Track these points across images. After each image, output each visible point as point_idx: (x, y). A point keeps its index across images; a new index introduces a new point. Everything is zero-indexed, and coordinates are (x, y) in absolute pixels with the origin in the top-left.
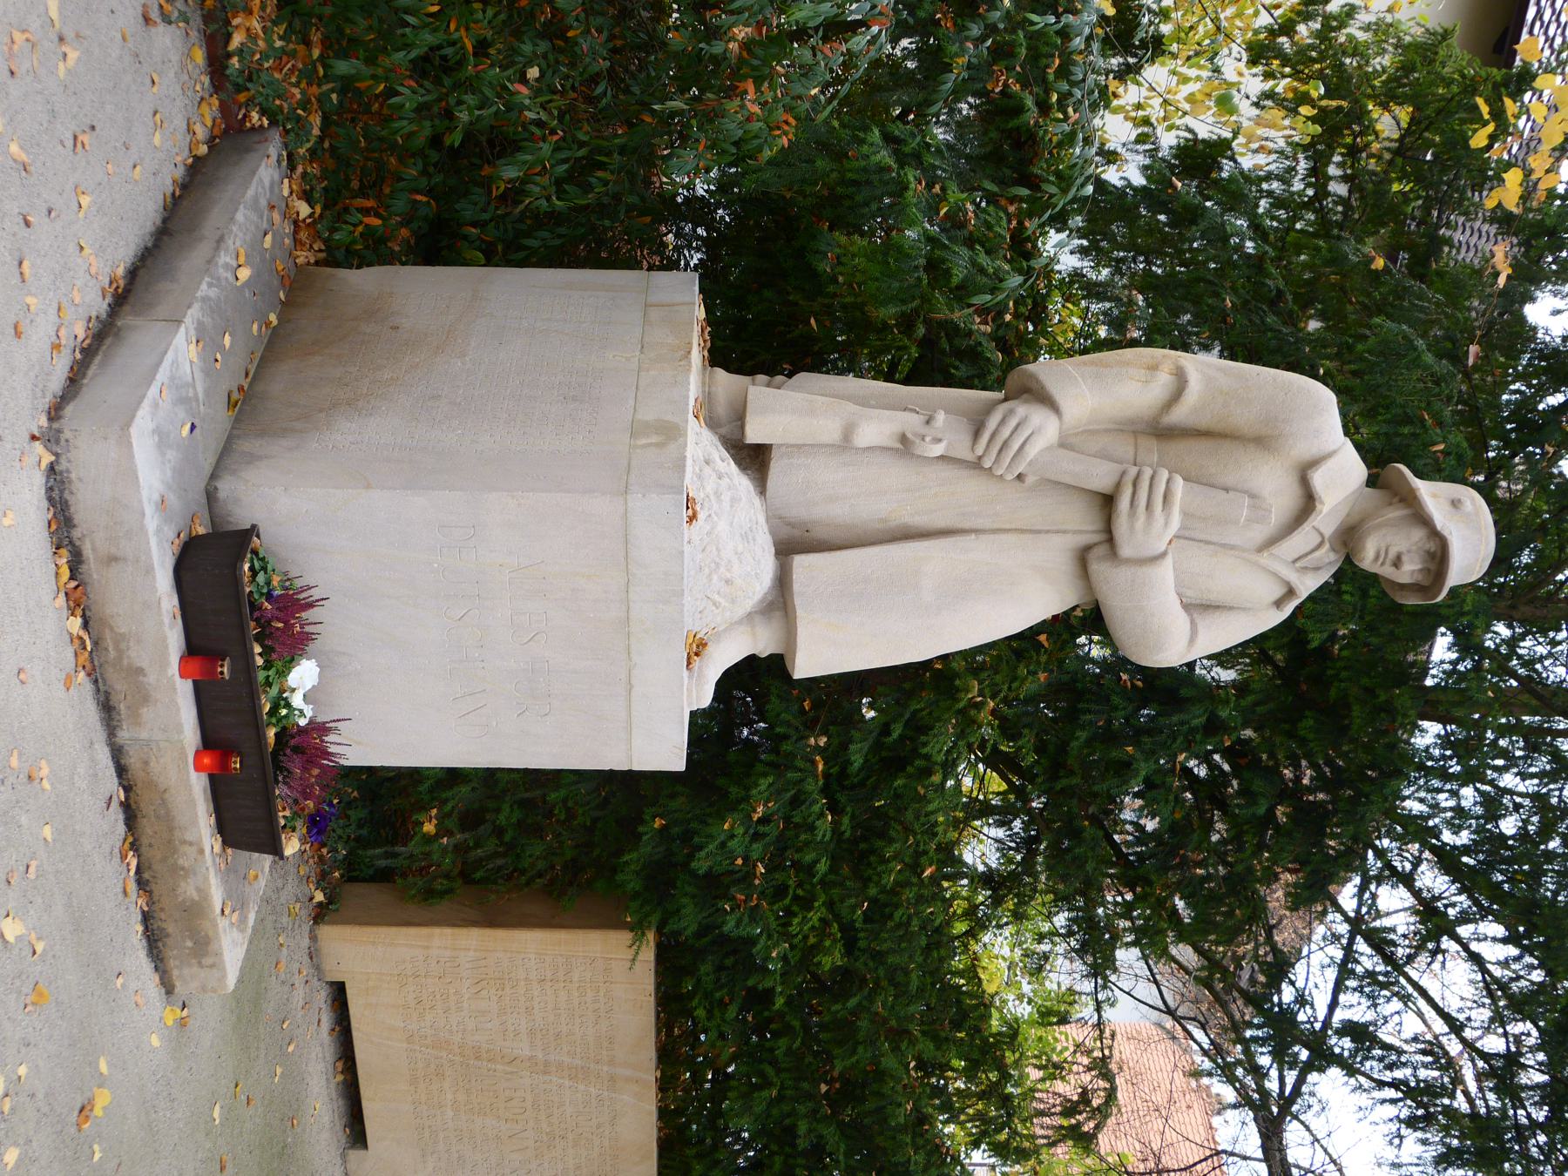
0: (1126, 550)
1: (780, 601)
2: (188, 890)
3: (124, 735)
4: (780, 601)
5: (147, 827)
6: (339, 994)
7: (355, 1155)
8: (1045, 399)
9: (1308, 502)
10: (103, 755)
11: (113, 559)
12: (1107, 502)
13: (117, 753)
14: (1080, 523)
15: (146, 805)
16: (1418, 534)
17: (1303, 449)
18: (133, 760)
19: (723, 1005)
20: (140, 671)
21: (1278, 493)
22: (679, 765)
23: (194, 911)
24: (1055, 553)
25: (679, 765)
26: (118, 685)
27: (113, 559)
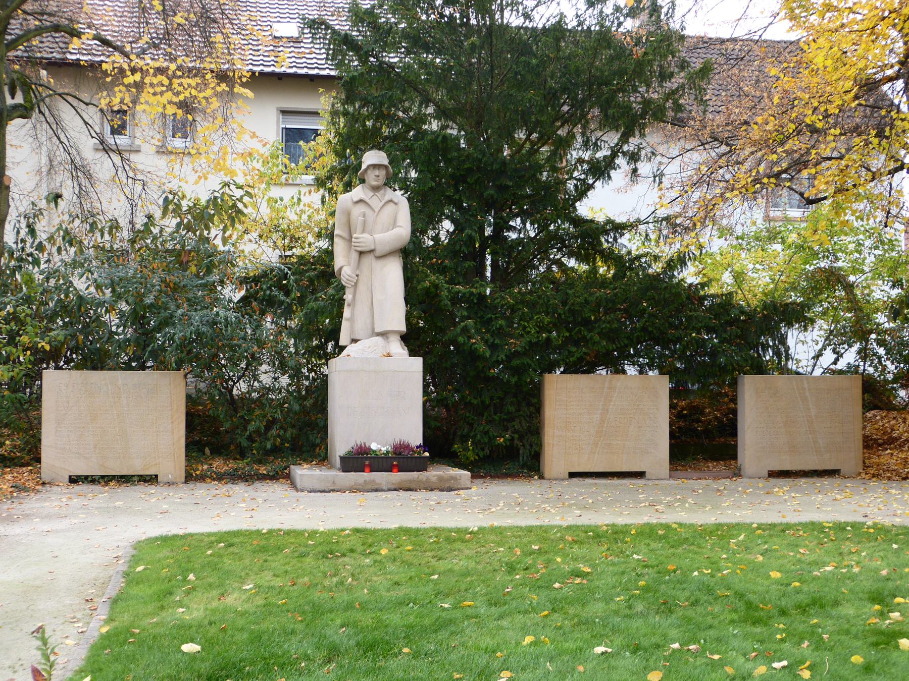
0: (372, 247)
1: (384, 334)
2: (434, 479)
3: (384, 488)
4: (384, 334)
5: (413, 486)
6: (572, 475)
7: (647, 475)
8: (341, 269)
9: (361, 201)
10: (390, 495)
11: (334, 482)
12: (361, 253)
13: (389, 490)
14: (368, 260)
15: (407, 486)
16: (369, 172)
17: (350, 204)
18: (393, 487)
19: (570, 352)
20: (365, 481)
21: (361, 208)
22: (421, 359)
23: (441, 479)
24: (377, 265)
25: (421, 359)
26: (369, 487)
27: (334, 482)
